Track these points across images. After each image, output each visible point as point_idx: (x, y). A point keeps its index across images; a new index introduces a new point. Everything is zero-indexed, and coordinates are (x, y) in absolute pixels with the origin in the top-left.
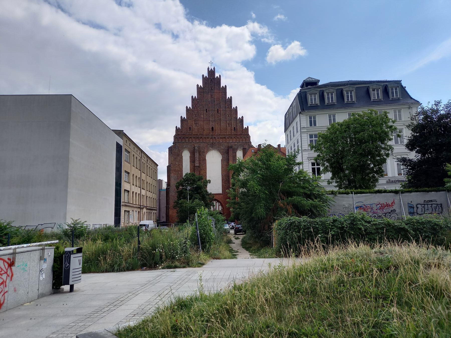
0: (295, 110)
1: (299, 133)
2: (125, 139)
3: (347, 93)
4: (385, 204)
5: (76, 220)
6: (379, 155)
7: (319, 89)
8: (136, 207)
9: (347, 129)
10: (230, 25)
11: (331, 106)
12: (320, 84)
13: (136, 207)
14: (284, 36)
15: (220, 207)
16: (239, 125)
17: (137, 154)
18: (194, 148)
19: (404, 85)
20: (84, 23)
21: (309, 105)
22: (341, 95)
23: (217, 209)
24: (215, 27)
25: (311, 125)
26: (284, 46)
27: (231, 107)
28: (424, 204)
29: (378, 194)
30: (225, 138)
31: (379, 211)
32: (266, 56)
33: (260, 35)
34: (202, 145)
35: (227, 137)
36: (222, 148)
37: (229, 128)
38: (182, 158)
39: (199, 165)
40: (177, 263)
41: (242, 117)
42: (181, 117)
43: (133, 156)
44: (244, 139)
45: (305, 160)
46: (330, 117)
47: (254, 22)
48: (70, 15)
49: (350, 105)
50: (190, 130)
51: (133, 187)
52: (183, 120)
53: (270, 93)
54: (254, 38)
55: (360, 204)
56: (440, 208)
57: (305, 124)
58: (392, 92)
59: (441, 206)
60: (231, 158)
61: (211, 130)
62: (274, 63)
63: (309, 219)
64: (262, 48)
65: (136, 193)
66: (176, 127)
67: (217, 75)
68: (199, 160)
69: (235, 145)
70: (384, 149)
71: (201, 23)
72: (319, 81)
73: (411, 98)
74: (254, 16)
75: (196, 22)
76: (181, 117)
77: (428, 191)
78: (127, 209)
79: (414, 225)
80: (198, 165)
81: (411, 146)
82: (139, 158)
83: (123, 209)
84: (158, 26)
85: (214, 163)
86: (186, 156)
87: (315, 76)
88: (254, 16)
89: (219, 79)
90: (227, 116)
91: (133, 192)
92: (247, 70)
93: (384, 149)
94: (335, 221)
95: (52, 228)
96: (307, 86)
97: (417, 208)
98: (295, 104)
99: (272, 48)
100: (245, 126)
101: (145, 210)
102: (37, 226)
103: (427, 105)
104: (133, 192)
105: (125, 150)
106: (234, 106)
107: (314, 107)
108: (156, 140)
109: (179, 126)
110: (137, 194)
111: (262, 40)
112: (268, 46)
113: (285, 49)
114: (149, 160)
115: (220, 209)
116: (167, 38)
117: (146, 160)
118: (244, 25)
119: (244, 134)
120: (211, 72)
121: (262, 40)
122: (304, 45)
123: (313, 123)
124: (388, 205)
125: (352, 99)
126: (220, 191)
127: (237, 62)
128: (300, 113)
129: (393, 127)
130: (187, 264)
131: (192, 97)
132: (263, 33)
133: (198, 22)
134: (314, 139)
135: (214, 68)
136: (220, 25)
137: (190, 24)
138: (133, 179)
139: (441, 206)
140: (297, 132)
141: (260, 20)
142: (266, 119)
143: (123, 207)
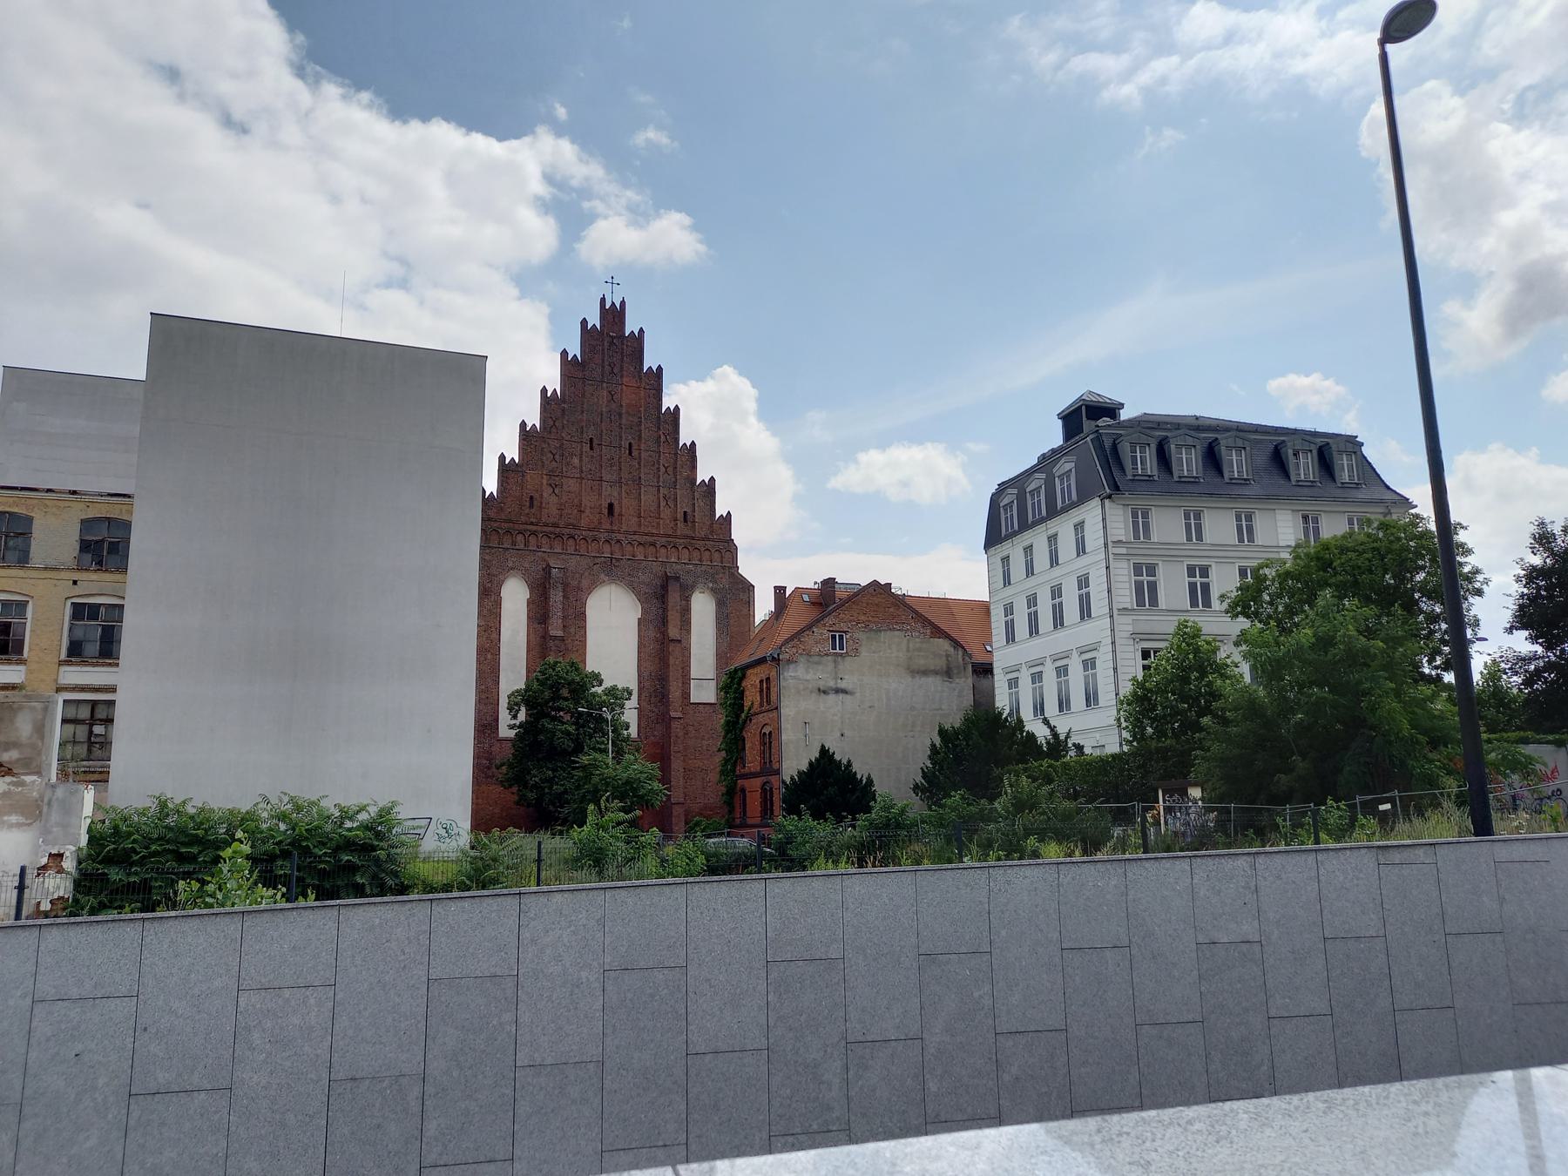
12: (1125, 415)
16: (700, 503)
22: (1212, 458)
24: (405, 122)
27: (677, 440)
30: (653, 544)
33: (574, 183)
34: (573, 562)
37: (666, 513)
44: (717, 555)
45: (1124, 642)
50: (531, 506)
67: (631, 326)
72: (1122, 406)
74: (561, 112)
75: (331, 90)
80: (560, 633)
84: (172, 74)
87: (1108, 391)
88: (561, 112)
89: (638, 340)
99: (601, 225)
100: (720, 511)
106: (685, 438)
119: (717, 539)
120: (613, 315)
132: (587, 179)
135: (623, 303)
136: (425, 118)
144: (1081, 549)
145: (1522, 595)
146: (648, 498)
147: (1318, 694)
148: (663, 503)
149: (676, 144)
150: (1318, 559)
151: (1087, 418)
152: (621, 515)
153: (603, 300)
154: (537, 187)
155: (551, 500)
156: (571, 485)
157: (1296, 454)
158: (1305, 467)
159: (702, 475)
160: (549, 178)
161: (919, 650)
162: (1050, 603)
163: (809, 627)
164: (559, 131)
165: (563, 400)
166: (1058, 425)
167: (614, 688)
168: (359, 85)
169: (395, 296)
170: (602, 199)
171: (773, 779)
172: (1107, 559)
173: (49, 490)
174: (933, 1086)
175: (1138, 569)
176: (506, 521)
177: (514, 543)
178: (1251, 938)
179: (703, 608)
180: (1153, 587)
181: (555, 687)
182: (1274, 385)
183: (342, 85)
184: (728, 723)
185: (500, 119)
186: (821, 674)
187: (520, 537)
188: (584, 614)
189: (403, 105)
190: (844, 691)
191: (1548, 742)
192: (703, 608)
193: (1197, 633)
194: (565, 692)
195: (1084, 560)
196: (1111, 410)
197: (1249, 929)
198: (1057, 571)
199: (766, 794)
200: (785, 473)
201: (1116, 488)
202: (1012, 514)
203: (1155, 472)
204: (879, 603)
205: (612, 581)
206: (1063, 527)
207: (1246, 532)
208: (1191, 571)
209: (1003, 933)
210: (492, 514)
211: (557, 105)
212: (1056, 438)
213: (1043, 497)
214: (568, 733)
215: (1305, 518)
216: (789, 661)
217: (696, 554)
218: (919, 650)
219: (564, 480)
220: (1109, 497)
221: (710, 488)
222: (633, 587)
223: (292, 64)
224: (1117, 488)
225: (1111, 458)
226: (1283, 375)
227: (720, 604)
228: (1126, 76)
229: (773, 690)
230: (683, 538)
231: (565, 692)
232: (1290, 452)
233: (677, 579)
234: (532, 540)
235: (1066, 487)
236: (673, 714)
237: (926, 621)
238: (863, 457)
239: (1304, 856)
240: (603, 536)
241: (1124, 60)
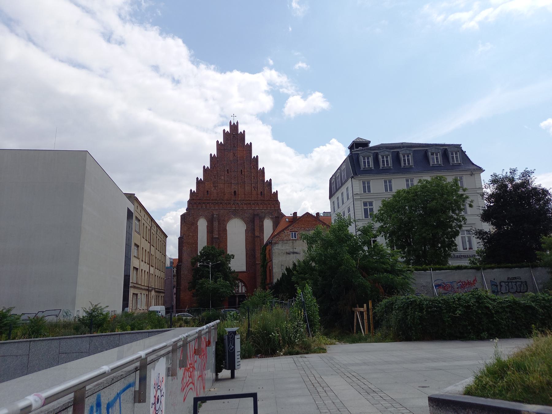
0: (344, 174)
1: (351, 200)
2: (136, 204)
3: (404, 157)
4: (467, 282)
5: (96, 306)
6: (451, 227)
7: (373, 152)
8: (145, 289)
9: (416, 197)
10: (243, 70)
11: (386, 171)
12: (371, 145)
13: (145, 289)
14: (305, 87)
15: (244, 288)
16: (267, 188)
17: (148, 223)
18: (213, 215)
19: (464, 149)
20: (62, 61)
21: (362, 169)
22: (397, 158)
23: (240, 291)
24: (225, 73)
25: (365, 191)
26: (305, 97)
27: (257, 167)
28: (508, 282)
29: (458, 271)
30: (250, 204)
31: (460, 290)
32: (284, 107)
33: (277, 84)
39: (218, 237)
40: (297, 349)
41: (270, 180)
42: (197, 178)
43: (144, 224)
47: (271, 69)
48: (44, 50)
49: (407, 170)
51: (142, 263)
52: (199, 182)
53: (290, 151)
54: (271, 87)
55: (439, 282)
56: (525, 286)
58: (451, 157)
59: (526, 284)
61: (233, 194)
62: (293, 115)
64: (280, 99)
65: (145, 271)
69: (262, 212)
70: (457, 220)
71: (208, 68)
73: (473, 164)
74: (271, 62)
75: (202, 66)
76: (197, 178)
77: (511, 268)
78: (136, 291)
79: (541, 303)
80: (217, 236)
81: (486, 216)
82: (149, 227)
83: (132, 291)
84: (156, 68)
85: (236, 233)
86: (202, 225)
88: (271, 62)
89: (243, 135)
90: (253, 178)
91: (142, 270)
92: (263, 123)
93: (457, 220)
94: (459, 299)
95: (57, 316)
96: (357, 147)
97: (501, 286)
98: (344, 167)
99: (291, 99)
100: (274, 190)
101: (153, 293)
102: (36, 314)
103: (501, 173)
104: (142, 270)
105: (137, 216)
106: (260, 166)
107: (368, 172)
108: (168, 206)
109: (194, 189)
110: (146, 273)
111: (281, 90)
112: (286, 97)
113: (305, 100)
114: (159, 231)
115: (244, 291)
116: (167, 83)
117: (156, 230)
119: (273, 200)
120: (234, 127)
121: (281, 90)
122: (327, 97)
123: (367, 188)
124: (469, 283)
125: (409, 163)
126: (244, 269)
127: (252, 115)
128: (352, 177)
129: (464, 196)
130: (307, 349)
131: (211, 155)
133: (205, 66)
134: (368, 207)
135: (237, 123)
136: (231, 71)
137: (194, 68)
138: (143, 254)
139: (526, 284)
140: (348, 198)
141: (278, 67)
142: (302, 183)
143: (132, 289)
147: (432, 250)
148: (253, 189)
151: (358, 147)
153: (230, 122)
160: (269, 84)
175: (365, 204)
176: (200, 200)
177: (202, 207)
187: (203, 205)
190: (297, 253)
196: (365, 144)
202: (335, 185)
205: (235, 217)
210: (194, 198)
216: (275, 243)
221: (270, 183)
223: (191, 61)
225: (367, 162)
226: (545, 120)
228: (472, 19)
232: (430, 153)
236: (257, 262)
241: (471, 13)
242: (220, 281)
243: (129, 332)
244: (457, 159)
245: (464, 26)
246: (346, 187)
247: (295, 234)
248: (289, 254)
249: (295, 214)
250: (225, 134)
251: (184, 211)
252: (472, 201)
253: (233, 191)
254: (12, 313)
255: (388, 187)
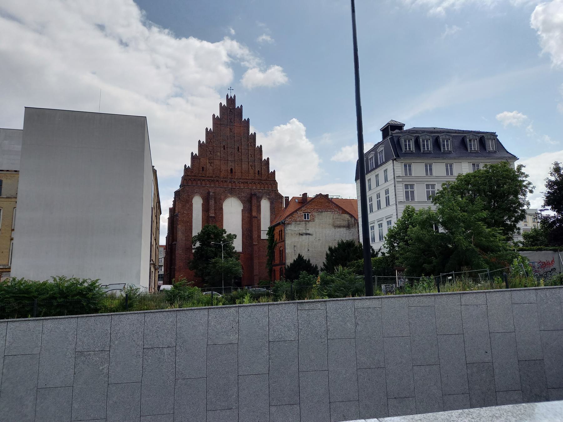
12: (405, 128)
16: (264, 167)
18: (209, 193)
22: (437, 144)
24: (180, 39)
27: (255, 145)
29: (539, 252)
30: (247, 183)
31: (540, 270)
33: (238, 56)
35: (249, 181)
36: (243, 195)
37: (251, 171)
38: (191, 205)
39: (213, 216)
44: (270, 186)
46: (426, 166)
50: (203, 170)
52: (194, 157)
57: (400, 173)
60: (254, 209)
63: (376, 283)
66: (185, 166)
67: (238, 105)
68: (215, 210)
71: (160, 32)
73: (508, 152)
74: (233, 32)
75: (155, 29)
80: (213, 215)
84: (101, 27)
86: (197, 203)
87: (399, 119)
88: (233, 32)
89: (240, 110)
99: (250, 71)
100: (271, 170)
107: (409, 154)
109: (189, 164)
116: (114, 45)
118: (218, 41)
119: (270, 180)
120: (231, 101)
121: (242, 63)
131: (207, 129)
132: (243, 54)
135: (235, 96)
136: (187, 37)
141: (238, 38)
144: (386, 180)
145: (549, 192)
146: (245, 166)
148: (250, 168)
149: (273, 40)
150: (466, 181)
152: (235, 172)
153: (227, 96)
154: (225, 58)
155: (210, 168)
156: (217, 162)
157: (470, 141)
158: (475, 146)
159: (264, 157)
160: (229, 55)
161: (337, 218)
162: (376, 200)
163: (296, 211)
164: (232, 38)
165: (213, 132)
166: (381, 133)
167: (230, 234)
168: (165, 28)
169: (179, 100)
170: (248, 61)
171: (283, 266)
172: (395, 183)
173: (7, 171)
174: (75, 406)
175: (406, 186)
178: (233, 342)
179: (265, 205)
180: (412, 192)
181: (209, 235)
182: (498, 116)
183: (159, 28)
184: (269, 246)
185: (210, 34)
186: (301, 228)
188: (222, 208)
189: (179, 32)
190: (309, 234)
191: (550, 250)
192: (265, 205)
193: (413, 210)
194: (212, 236)
195: (387, 184)
196: (400, 127)
197: (233, 338)
198: (379, 188)
199: (281, 271)
200: (316, 156)
201: (398, 156)
203: (414, 150)
204: (323, 202)
206: (380, 171)
207: (449, 170)
208: (428, 186)
209: (116, 342)
210: (189, 174)
211: (231, 29)
212: (380, 139)
213: (374, 161)
214: (212, 251)
215: (474, 165)
216: (288, 224)
217: (262, 185)
218: (337, 218)
219: (215, 161)
220: (395, 159)
221: (267, 162)
222: (240, 198)
223: (142, 21)
224: (399, 156)
227: (272, 203)
229: (283, 234)
230: (258, 180)
231: (212, 236)
232: (468, 140)
233: (255, 195)
234: (203, 182)
235: (381, 157)
236: (254, 243)
237: (338, 206)
238: (344, 149)
239: (263, 307)
240: (229, 181)
242: (232, 261)
243: (247, 304)
244: (427, 146)
245: (431, 11)
246: (385, 169)
247: (308, 215)
248: (302, 235)
249: (305, 195)
250: (222, 108)
251: (178, 188)
252: (534, 187)
253: (229, 169)
254: (97, 284)
255: (449, 170)
